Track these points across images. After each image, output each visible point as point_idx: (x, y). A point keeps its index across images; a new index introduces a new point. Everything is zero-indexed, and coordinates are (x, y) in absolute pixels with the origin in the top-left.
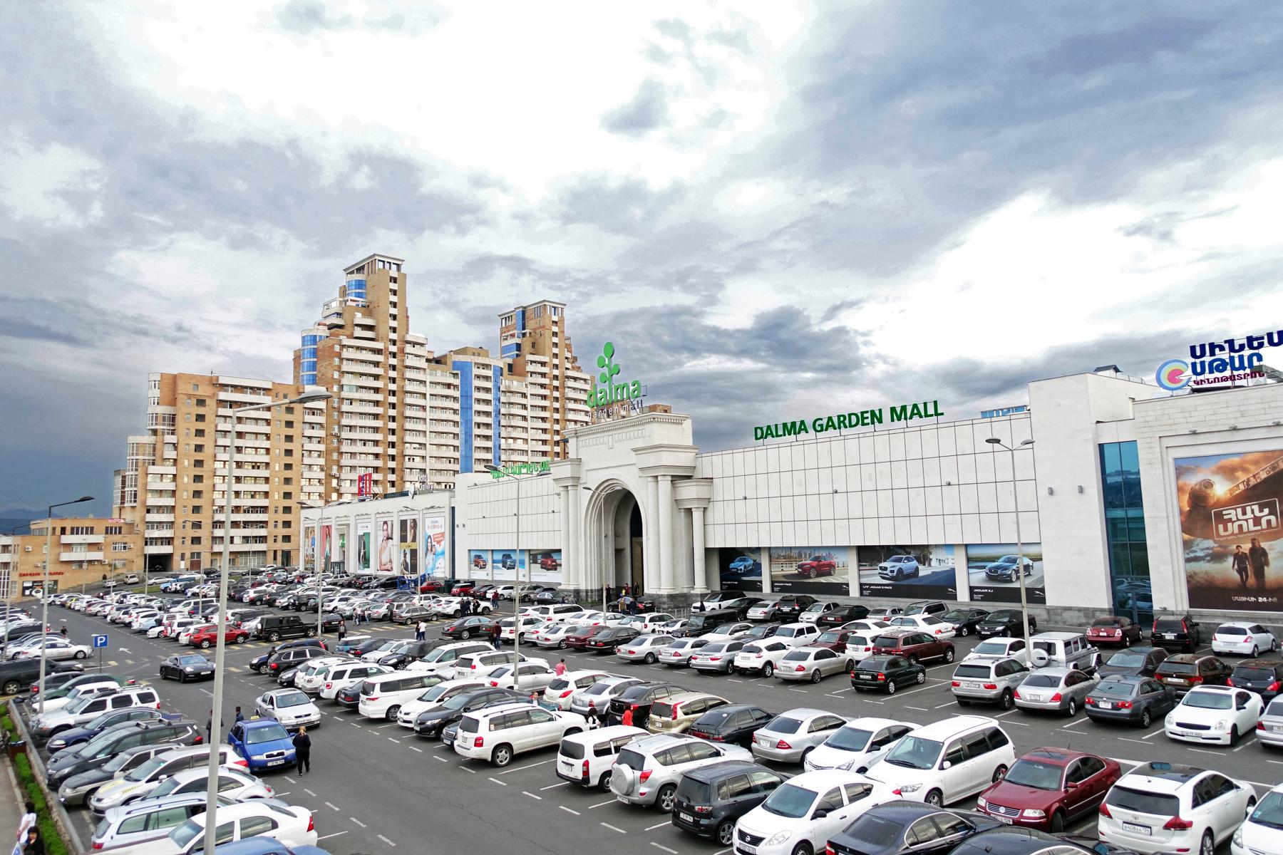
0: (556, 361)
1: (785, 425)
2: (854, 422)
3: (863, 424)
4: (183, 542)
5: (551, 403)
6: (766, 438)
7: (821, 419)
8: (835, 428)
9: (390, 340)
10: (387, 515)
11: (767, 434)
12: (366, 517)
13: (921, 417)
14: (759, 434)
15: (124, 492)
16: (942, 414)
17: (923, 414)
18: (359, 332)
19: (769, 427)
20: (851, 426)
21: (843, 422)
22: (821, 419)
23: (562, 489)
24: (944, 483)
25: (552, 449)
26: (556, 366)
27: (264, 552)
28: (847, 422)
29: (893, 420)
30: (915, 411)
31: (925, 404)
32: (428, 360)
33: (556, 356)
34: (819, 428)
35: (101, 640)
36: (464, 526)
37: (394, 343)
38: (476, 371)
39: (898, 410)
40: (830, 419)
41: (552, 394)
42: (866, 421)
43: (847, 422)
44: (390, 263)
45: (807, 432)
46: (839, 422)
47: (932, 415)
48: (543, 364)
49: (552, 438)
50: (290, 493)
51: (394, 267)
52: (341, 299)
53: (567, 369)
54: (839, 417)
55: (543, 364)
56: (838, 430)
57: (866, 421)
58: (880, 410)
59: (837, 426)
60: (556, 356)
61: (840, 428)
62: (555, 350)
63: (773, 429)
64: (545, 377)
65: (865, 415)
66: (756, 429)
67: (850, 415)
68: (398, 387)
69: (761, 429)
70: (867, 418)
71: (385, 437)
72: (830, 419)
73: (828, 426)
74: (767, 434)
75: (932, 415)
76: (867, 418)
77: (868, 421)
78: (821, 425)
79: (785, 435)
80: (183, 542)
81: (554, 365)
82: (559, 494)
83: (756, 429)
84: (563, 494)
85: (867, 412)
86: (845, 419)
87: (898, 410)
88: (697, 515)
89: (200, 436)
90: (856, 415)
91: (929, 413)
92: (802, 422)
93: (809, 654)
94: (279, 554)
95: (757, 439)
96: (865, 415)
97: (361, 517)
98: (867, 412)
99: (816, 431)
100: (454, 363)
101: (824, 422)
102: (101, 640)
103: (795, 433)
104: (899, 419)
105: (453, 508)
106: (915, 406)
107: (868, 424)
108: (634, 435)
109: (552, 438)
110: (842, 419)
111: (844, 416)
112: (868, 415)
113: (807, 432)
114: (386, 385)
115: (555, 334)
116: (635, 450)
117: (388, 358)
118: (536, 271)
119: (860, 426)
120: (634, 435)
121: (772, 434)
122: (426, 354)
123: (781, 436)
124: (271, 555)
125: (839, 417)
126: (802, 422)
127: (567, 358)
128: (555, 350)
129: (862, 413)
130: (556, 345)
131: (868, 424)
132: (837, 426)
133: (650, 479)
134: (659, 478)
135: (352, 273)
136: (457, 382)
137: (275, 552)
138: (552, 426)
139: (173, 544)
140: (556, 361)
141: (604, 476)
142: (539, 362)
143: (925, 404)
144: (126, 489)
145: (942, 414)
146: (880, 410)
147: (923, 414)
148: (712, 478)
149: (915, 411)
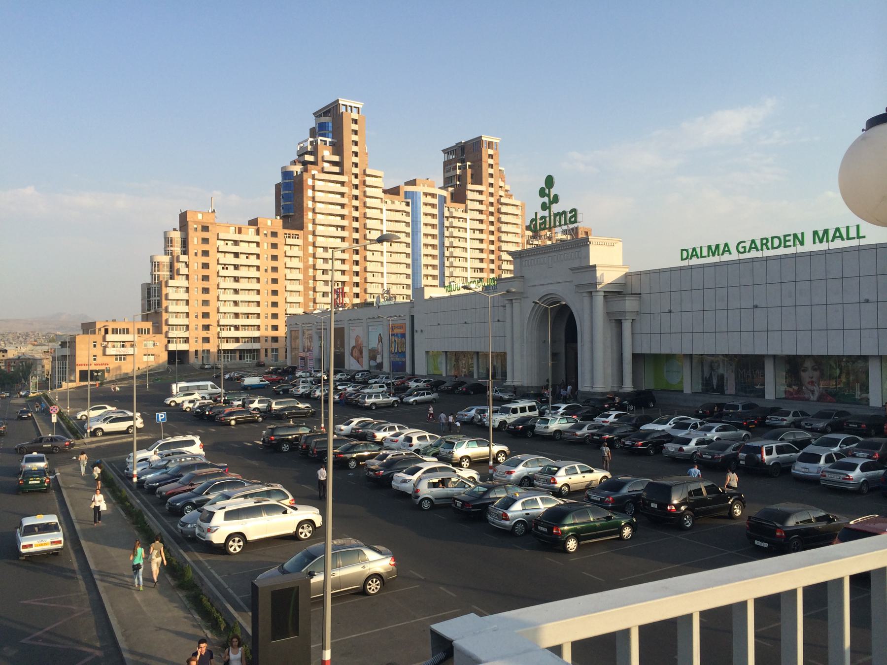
0: (491, 190)
1: (709, 247)
2: (776, 245)
3: (785, 246)
4: (196, 341)
5: (488, 226)
6: (691, 259)
7: (744, 242)
8: (758, 250)
9: (353, 174)
10: (339, 323)
11: (692, 256)
12: (358, 321)
13: (698, 258)
14: (685, 256)
15: (150, 301)
16: (864, 237)
17: (699, 255)
18: (327, 166)
19: (694, 249)
20: (773, 248)
21: (766, 244)
22: (744, 242)
23: (507, 302)
24: (862, 300)
25: (488, 266)
26: (491, 195)
27: (257, 351)
28: (769, 245)
29: (814, 243)
30: (753, 246)
31: (848, 228)
32: (385, 192)
33: (491, 185)
34: (742, 250)
35: (162, 416)
36: (422, 331)
37: (356, 176)
38: (423, 199)
39: (821, 234)
40: (753, 241)
41: (488, 219)
42: (788, 244)
43: (769, 245)
44: (351, 107)
45: (730, 253)
46: (762, 245)
47: (854, 238)
48: (481, 192)
49: (488, 257)
50: (208, 314)
51: (354, 110)
52: (312, 139)
53: (501, 196)
54: (762, 239)
55: (481, 192)
56: (761, 252)
57: (788, 244)
58: (803, 234)
59: (759, 248)
60: (491, 185)
61: (762, 250)
62: (491, 180)
63: (698, 251)
64: (482, 204)
65: (787, 238)
66: (682, 250)
67: (773, 238)
68: (360, 214)
69: (687, 250)
70: (789, 241)
71: (351, 257)
72: (753, 241)
73: (751, 248)
74: (692, 256)
75: (854, 238)
76: (789, 241)
77: (791, 243)
78: (744, 248)
79: (709, 256)
80: (196, 341)
81: (490, 193)
82: (504, 306)
83: (682, 250)
84: (508, 306)
85: (789, 235)
86: (768, 242)
87: (821, 234)
88: (627, 326)
89: (206, 256)
90: (779, 238)
91: (703, 255)
92: (726, 245)
93: (857, 465)
94: (269, 351)
95: (682, 259)
96: (787, 238)
97: (354, 322)
98: (789, 235)
99: (739, 252)
100: (406, 192)
101: (747, 245)
102: (162, 416)
103: (718, 255)
104: (821, 241)
105: (413, 317)
106: (837, 230)
107: (790, 246)
108: (531, 263)
109: (488, 257)
110: (765, 241)
111: (767, 239)
112: (791, 238)
113: (730, 253)
114: (350, 212)
115: (491, 166)
116: (572, 269)
117: (351, 190)
118: (302, 172)
119: (782, 248)
120: (531, 263)
121: (696, 255)
122: (382, 185)
123: (705, 257)
124: (263, 352)
125: (762, 239)
126: (726, 245)
127: (501, 187)
128: (491, 180)
129: (785, 236)
130: (491, 175)
131: (790, 246)
132: (759, 248)
133: (585, 294)
134: (514, 301)
135: (320, 116)
136: (409, 209)
137: (266, 350)
138: (488, 246)
139: (188, 343)
140: (491, 190)
141: (543, 291)
142: (477, 191)
143: (848, 228)
144: (151, 299)
145: (864, 237)
146: (803, 234)
147: (699, 255)
148: (640, 294)
149: (694, 253)
